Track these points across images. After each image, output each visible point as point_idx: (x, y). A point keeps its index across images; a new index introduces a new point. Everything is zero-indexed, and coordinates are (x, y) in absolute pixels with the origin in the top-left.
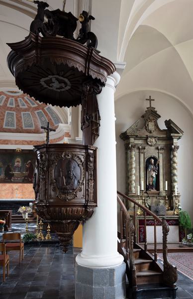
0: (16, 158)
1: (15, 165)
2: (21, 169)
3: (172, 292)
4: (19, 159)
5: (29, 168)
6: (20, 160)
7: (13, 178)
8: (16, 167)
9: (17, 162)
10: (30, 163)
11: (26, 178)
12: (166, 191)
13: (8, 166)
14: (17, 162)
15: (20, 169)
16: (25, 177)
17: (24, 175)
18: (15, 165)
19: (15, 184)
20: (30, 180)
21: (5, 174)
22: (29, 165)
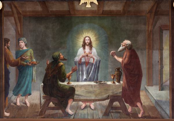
0: (79, 33)
1: (77, 59)
2: (97, 68)
3: (40, 2)
4: (88, 35)
5: (127, 66)
6: (93, 39)
7: (71, 103)
8: (80, 63)
9: (84, 46)
10: (130, 48)
11: (116, 104)
12: (48, 64)
13: (56, 60)
14: (84, 46)
15: (95, 70)
16: (113, 98)
17: (110, 93)
18: (77, 59)
19: (169, 39)
20: (130, 109)
21: (44, 88)
22: (127, 54)
